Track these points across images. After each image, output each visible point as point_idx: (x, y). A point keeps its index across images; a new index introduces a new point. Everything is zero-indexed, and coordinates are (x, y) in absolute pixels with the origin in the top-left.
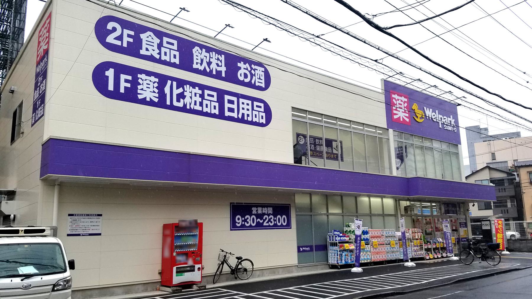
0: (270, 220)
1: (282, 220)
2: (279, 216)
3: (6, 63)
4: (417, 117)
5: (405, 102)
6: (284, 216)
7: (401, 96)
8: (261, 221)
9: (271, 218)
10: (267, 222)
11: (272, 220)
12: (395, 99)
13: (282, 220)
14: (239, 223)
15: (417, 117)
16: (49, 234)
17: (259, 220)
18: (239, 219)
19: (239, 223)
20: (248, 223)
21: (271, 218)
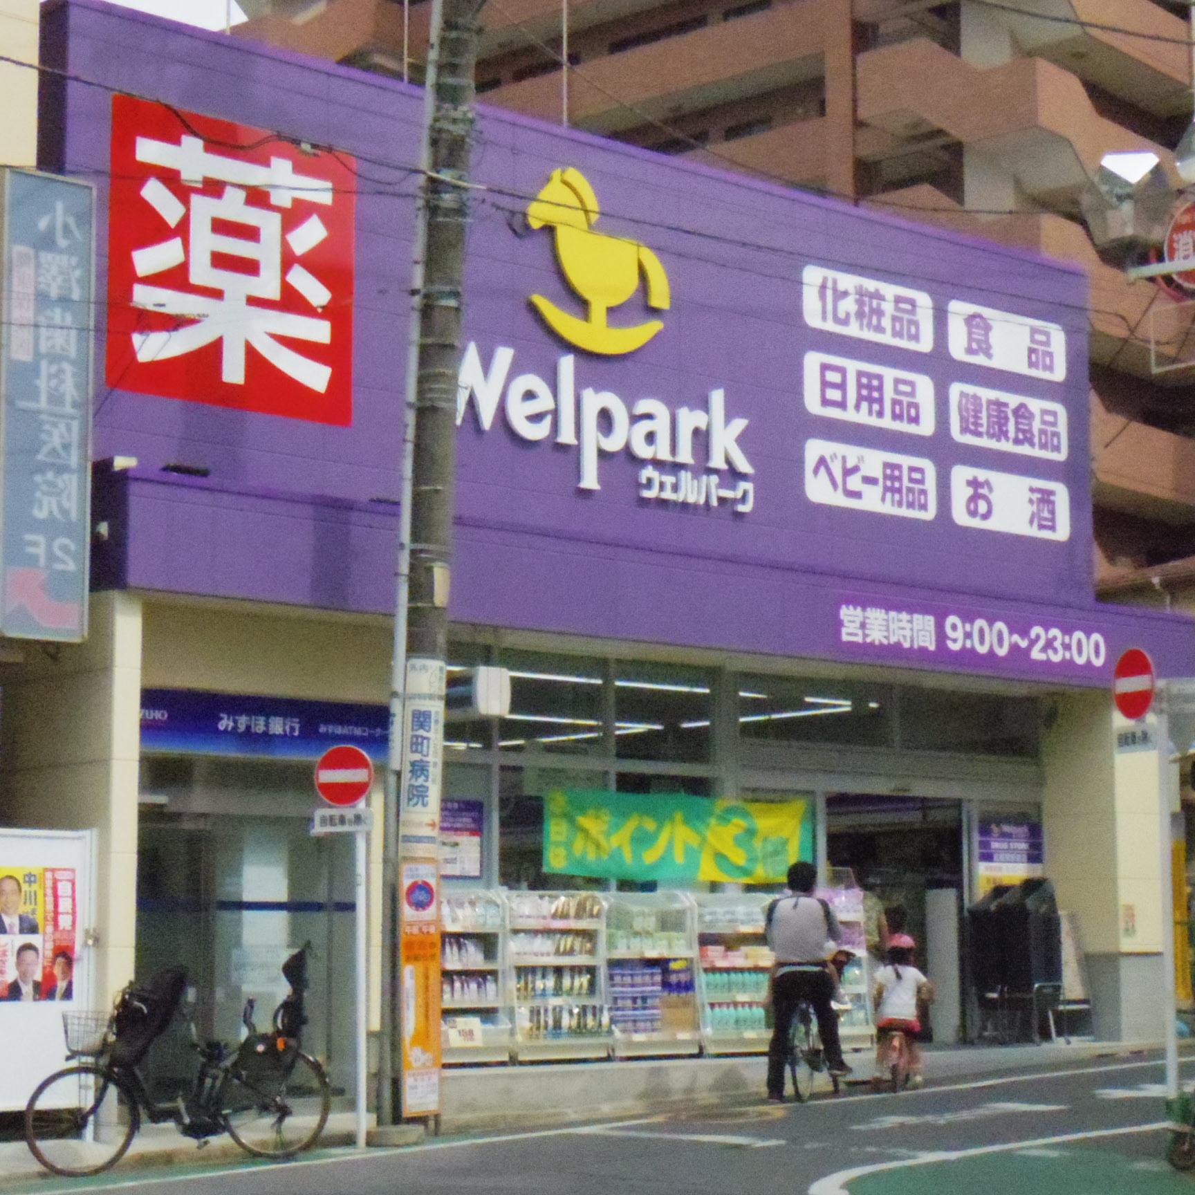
0: (1049, 644)
1: (1088, 649)
2: (980, 623)
3: (1190, 897)
4: (580, 305)
5: (294, 216)
6: (1096, 637)
7: (255, 154)
8: (1024, 644)
9: (1055, 638)
10: (1044, 650)
11: (1057, 644)
12: (170, 178)
13: (1088, 649)
14: (955, 641)
15: (580, 305)
16: (1097, 242)
17: (1016, 638)
18: (954, 627)
19: (955, 641)
20: (1055, 651)
21: (1055, 638)
